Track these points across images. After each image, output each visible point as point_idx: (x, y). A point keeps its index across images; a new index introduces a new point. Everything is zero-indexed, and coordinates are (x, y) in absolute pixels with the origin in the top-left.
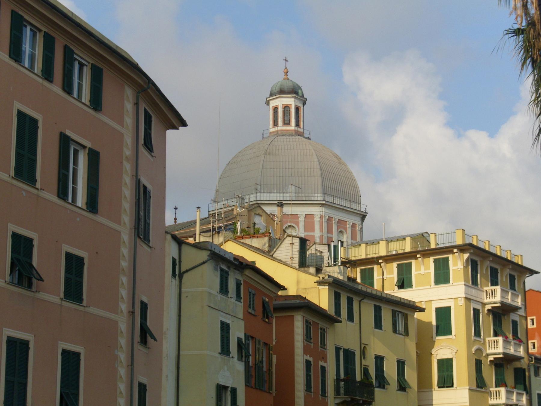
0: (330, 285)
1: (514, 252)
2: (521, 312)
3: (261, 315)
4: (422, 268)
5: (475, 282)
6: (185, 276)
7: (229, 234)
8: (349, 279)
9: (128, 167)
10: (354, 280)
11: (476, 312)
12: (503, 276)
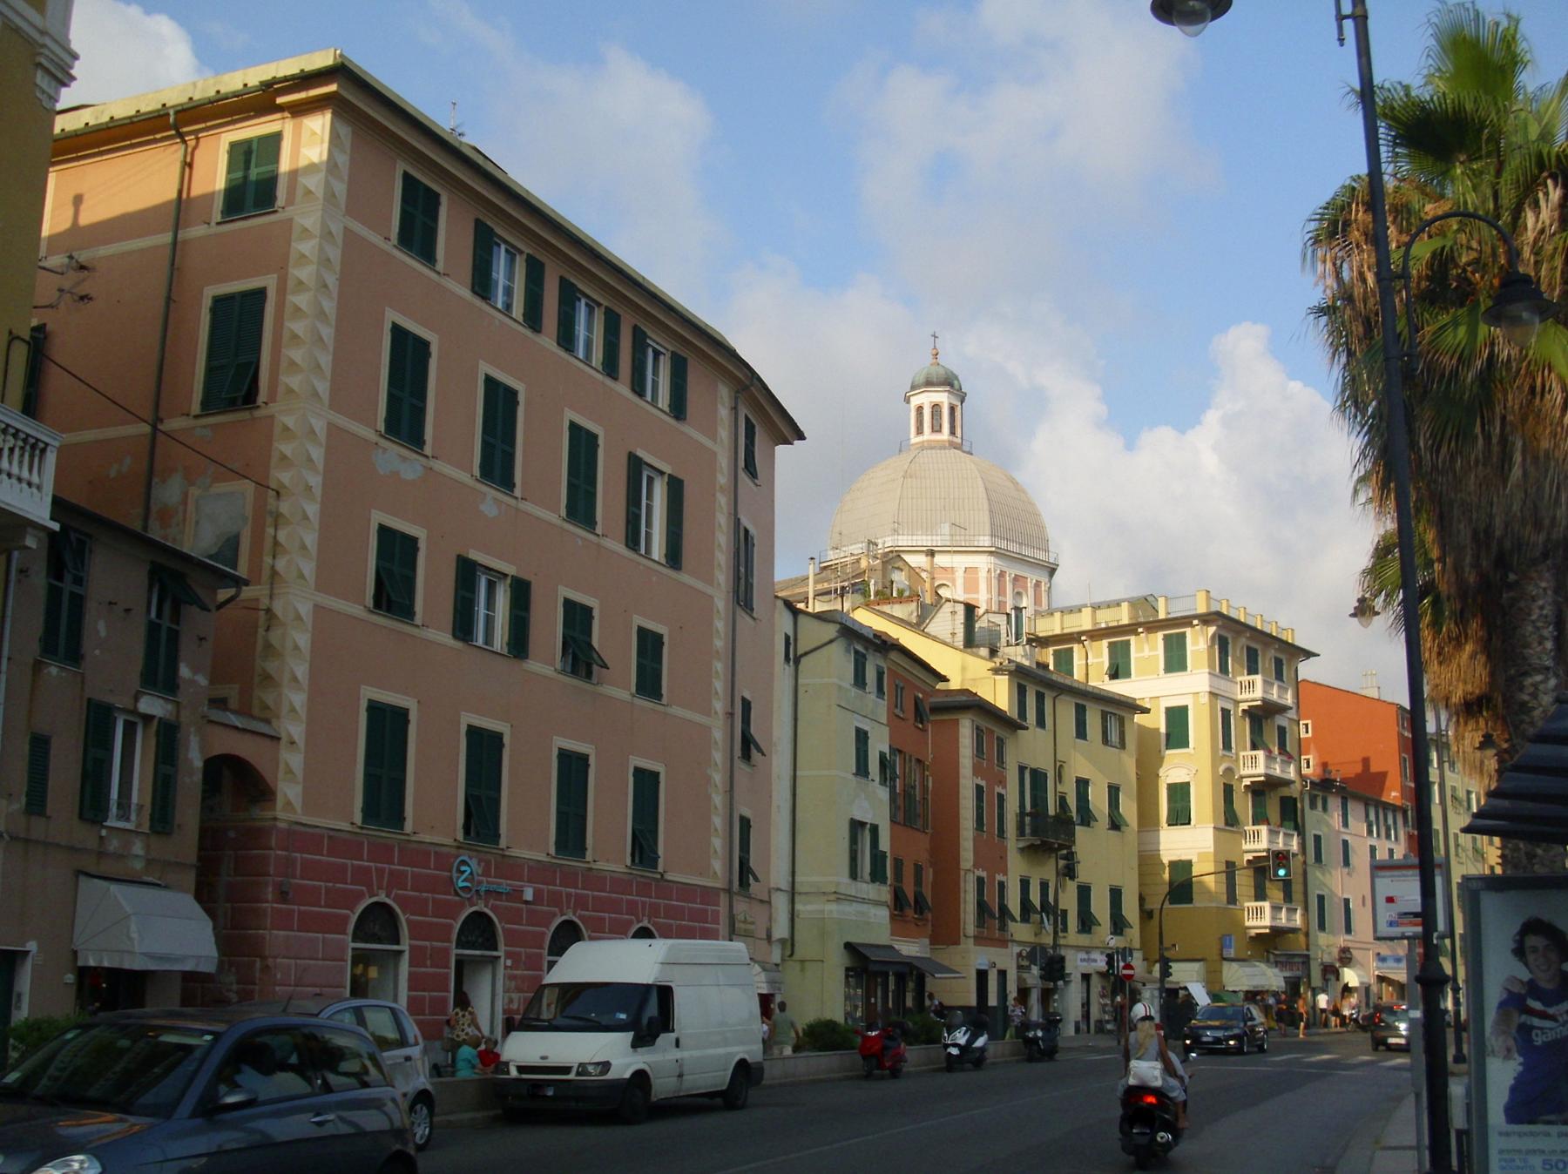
0: (1011, 673)
1: (1282, 624)
2: (1292, 714)
3: (912, 720)
4: (1146, 647)
5: (1224, 669)
6: (804, 661)
7: (859, 598)
8: (1038, 664)
9: (723, 500)
10: (1046, 666)
11: (1226, 714)
12: (1266, 660)
